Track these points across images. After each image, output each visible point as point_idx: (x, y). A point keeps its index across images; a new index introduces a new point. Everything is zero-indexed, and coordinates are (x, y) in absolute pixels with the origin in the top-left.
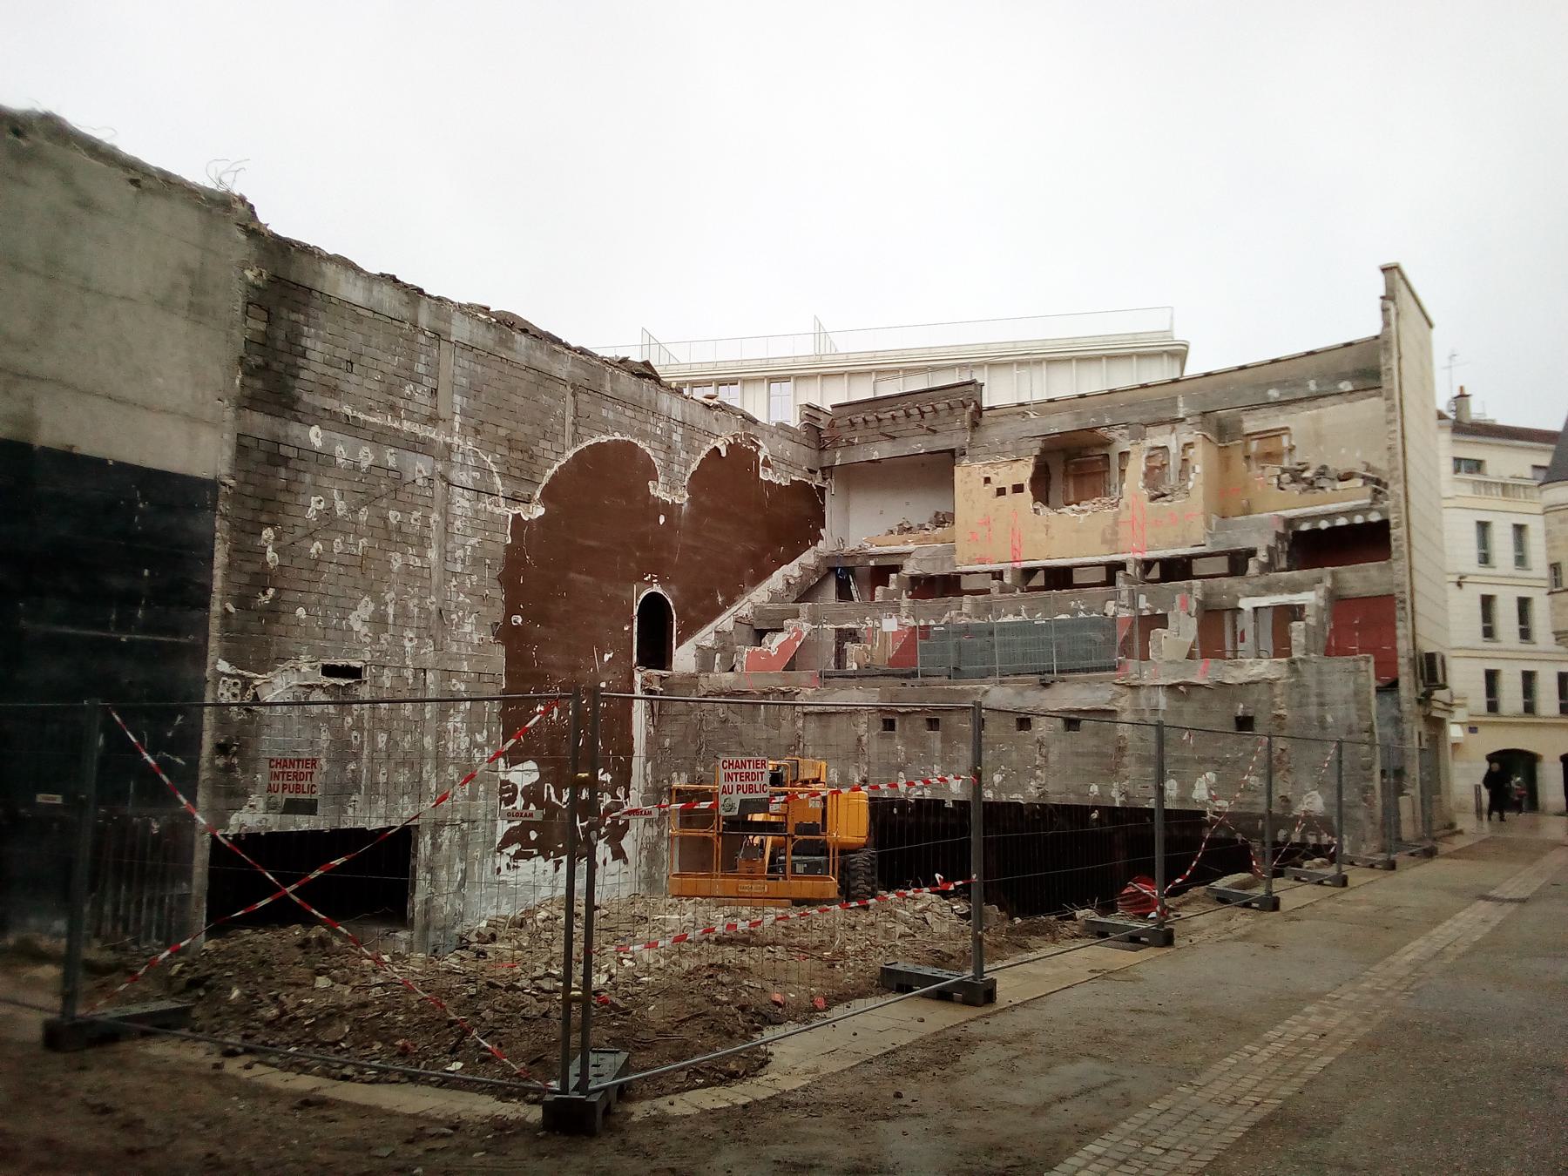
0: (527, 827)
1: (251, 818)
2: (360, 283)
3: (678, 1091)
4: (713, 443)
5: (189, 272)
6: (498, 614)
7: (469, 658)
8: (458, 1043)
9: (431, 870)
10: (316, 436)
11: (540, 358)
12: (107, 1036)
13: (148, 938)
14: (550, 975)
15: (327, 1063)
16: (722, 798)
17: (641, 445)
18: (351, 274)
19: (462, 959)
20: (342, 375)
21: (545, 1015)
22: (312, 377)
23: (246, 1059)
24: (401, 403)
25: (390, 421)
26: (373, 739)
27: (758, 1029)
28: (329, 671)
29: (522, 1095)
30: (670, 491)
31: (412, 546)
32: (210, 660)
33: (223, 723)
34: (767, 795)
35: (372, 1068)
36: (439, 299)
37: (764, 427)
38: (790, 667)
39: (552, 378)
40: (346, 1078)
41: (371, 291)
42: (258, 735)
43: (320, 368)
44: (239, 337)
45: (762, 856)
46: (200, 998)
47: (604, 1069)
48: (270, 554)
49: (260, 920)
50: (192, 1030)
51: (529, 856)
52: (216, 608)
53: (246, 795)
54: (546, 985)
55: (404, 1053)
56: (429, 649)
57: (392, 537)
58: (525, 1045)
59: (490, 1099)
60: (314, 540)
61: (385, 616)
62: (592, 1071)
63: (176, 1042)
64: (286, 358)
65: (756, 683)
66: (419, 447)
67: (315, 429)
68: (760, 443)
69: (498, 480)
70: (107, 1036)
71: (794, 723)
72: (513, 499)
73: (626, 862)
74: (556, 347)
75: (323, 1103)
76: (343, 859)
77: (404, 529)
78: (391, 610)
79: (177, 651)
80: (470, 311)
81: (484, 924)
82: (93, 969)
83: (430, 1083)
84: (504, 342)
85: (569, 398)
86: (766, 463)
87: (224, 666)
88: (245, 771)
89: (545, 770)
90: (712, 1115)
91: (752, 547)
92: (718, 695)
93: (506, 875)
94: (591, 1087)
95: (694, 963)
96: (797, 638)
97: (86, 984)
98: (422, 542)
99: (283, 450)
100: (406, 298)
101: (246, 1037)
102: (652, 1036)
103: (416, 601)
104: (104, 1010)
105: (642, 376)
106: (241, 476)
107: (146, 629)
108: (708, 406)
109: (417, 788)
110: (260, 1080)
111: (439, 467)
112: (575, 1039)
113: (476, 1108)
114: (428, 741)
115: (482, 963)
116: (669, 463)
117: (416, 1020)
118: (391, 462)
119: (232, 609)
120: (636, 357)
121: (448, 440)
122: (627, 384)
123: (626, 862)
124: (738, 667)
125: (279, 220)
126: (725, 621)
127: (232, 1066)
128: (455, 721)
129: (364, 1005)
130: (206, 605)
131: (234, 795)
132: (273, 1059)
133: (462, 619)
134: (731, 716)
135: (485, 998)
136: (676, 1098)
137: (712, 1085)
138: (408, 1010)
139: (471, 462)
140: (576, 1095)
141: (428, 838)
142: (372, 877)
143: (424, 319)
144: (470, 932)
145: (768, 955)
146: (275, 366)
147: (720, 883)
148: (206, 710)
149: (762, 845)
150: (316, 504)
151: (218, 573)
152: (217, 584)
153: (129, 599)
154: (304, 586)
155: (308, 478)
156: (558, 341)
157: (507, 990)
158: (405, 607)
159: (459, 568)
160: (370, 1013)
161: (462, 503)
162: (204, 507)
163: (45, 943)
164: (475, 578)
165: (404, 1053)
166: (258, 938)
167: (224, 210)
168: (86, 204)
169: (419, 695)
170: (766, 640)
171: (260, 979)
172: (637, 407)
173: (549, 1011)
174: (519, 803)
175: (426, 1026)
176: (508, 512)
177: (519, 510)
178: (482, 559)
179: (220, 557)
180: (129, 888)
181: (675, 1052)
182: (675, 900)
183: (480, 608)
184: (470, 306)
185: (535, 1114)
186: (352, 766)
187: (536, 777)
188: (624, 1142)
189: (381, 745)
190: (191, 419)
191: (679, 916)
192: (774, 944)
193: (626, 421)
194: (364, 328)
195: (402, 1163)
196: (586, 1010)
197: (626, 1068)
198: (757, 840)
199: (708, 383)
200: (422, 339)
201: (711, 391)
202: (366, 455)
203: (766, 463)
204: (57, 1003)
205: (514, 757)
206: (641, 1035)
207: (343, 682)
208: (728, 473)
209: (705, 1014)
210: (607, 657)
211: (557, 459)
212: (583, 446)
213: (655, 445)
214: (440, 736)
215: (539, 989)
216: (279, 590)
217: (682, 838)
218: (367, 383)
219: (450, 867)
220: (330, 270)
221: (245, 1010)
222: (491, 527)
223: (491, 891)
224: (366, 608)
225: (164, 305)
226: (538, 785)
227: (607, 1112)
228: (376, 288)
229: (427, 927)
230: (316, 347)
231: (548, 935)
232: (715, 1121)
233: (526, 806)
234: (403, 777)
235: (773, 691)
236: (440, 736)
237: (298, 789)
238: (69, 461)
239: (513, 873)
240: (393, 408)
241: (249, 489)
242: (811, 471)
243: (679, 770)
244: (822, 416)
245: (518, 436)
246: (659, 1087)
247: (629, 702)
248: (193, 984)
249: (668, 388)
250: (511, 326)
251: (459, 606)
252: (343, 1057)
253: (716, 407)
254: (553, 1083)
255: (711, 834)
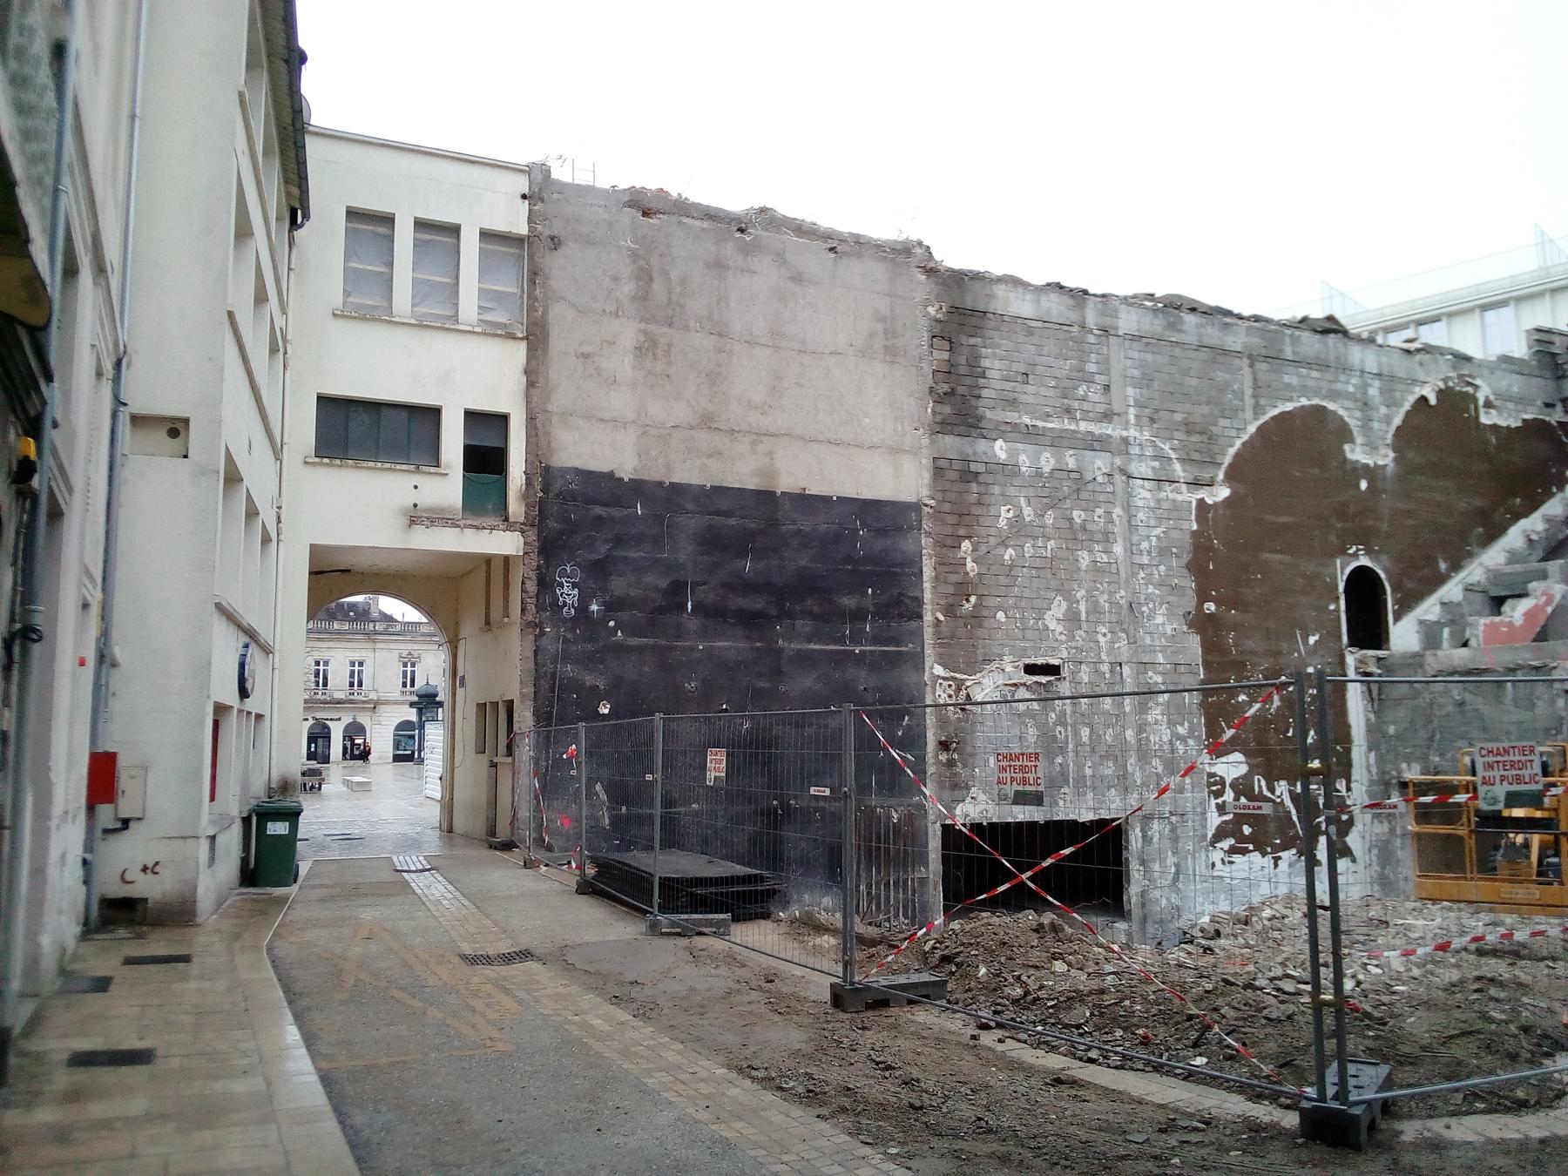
0: (1240, 819)
1: (976, 808)
2: (1029, 297)
3: (1453, 1114)
4: (1419, 391)
5: (882, 319)
6: (1190, 602)
7: (1163, 650)
8: (1199, 1038)
9: (1143, 862)
10: (1000, 449)
11: (1212, 334)
12: (881, 1002)
13: (896, 916)
14: (1288, 976)
15: (1073, 1044)
16: (1482, 790)
17: (1331, 406)
18: (1020, 290)
19: (1189, 953)
20: (1019, 387)
21: (1289, 1017)
22: (993, 394)
23: (999, 1033)
24: (1076, 405)
25: (1069, 425)
26: (1076, 733)
27: (1548, 1055)
28: (1031, 669)
29: (1274, 1098)
30: (1370, 451)
31: (1098, 542)
32: (927, 665)
33: (943, 722)
34: (1540, 787)
35: (1116, 1053)
36: (1104, 296)
37: (1481, 364)
38: (1542, 636)
39: (1226, 352)
40: (1091, 1061)
41: (1038, 302)
42: (974, 732)
43: (998, 385)
44: (928, 370)
45: (1528, 857)
46: (953, 973)
47: (1363, 1080)
48: (970, 565)
49: (993, 904)
50: (949, 1002)
51: (1244, 852)
52: (928, 618)
53: (968, 788)
54: (1288, 986)
55: (1145, 1041)
56: (1122, 643)
57: (1077, 536)
58: (1271, 1047)
59: (1240, 1098)
60: (1007, 547)
61: (1078, 613)
62: (1352, 1082)
63: (936, 1011)
64: (968, 381)
65: (1499, 658)
66: (1097, 445)
67: (1000, 442)
68: (1478, 382)
69: (1178, 467)
70: (881, 1002)
71: (1553, 702)
72: (1196, 484)
73: (1354, 861)
74: (1228, 320)
75: (1074, 1083)
76: (1071, 849)
77: (1089, 527)
78: (1083, 607)
79: (895, 660)
80: (1134, 301)
81: (1206, 919)
82: (863, 941)
83: (1176, 1075)
84: (1173, 326)
85: (1246, 370)
86: (1488, 404)
87: (939, 670)
88: (965, 766)
89: (1255, 761)
90: (1503, 1147)
91: (1479, 502)
92: (1451, 674)
93: (1221, 870)
94: (1352, 1098)
95: (1455, 975)
96: (1548, 603)
97: (859, 955)
98: (1107, 538)
99: (973, 467)
100: (1072, 302)
101: (996, 1012)
102: (1417, 1051)
103: (1106, 597)
104: (875, 978)
105: (1325, 332)
106: (939, 496)
107: (875, 640)
108: (1408, 351)
109: (1123, 782)
110: (1013, 1054)
111: (1118, 461)
112: (1330, 1045)
113: (1226, 1105)
114: (1130, 734)
115: (1210, 959)
116: (1366, 423)
117: (1154, 1011)
118: (1071, 463)
119: (941, 618)
120: (1317, 313)
121: (1125, 434)
122: (1310, 344)
123: (1354, 861)
124: (1473, 642)
125: (951, 257)
126: (1452, 590)
127: (988, 1038)
128: (1155, 714)
129: (1102, 992)
130: (920, 617)
131: (957, 788)
132: (1024, 1036)
133: (1153, 611)
134: (1468, 697)
135: (1223, 994)
136: (1453, 1121)
137: (1496, 1111)
138: (1144, 998)
139: (1149, 452)
140: (1335, 1105)
141: (1138, 830)
142: (1085, 867)
143: (1091, 319)
144: (1193, 926)
145: (1546, 971)
146: (961, 390)
147: (1476, 887)
148: (928, 710)
149: (1526, 845)
150: (1006, 513)
151: (927, 586)
152: (928, 596)
153: (858, 616)
154: (1002, 591)
155: (996, 490)
156: (1229, 313)
157: (1245, 987)
158: (1096, 604)
159: (1145, 560)
160: (1109, 1000)
161: (1143, 494)
162: (911, 528)
163: (823, 917)
164: (1162, 568)
165: (1145, 1041)
166: (995, 920)
167: (906, 256)
168: (797, 278)
169: (1118, 689)
170: (1506, 608)
171: (1003, 960)
172: (1323, 366)
173: (1294, 1014)
174: (1229, 796)
175: (1165, 1017)
176: (1192, 497)
177: (1202, 494)
178: (1168, 549)
179: (928, 573)
180: (878, 872)
181: (1446, 1071)
182: (1419, 904)
183: (1171, 598)
184: (1135, 297)
185: (1291, 1120)
186: (1059, 760)
187: (1244, 769)
188: (1395, 1162)
189: (1085, 739)
190: (895, 450)
191: (1429, 923)
192: (1554, 959)
193: (1311, 383)
194: (1036, 339)
195: (1158, 1151)
196: (1339, 1014)
197: (1388, 1083)
198: (1520, 839)
199: (1404, 326)
200: (1091, 339)
201: (1409, 333)
202: (1047, 461)
203: (1488, 404)
204: (840, 969)
205: (1218, 750)
206: (1406, 1049)
207: (1044, 679)
208: (1441, 425)
209: (1478, 1032)
210: (1312, 640)
211: (1238, 436)
212: (1266, 418)
213: (1348, 404)
214: (1141, 728)
215: (1278, 990)
216: (980, 596)
217: (1419, 837)
218: (1043, 391)
219: (1163, 861)
220: (1000, 290)
221: (993, 988)
222: (1175, 515)
223: (1210, 888)
224: (1059, 608)
225: (864, 353)
226: (1247, 778)
227: (1372, 1126)
228: (1044, 298)
229: (1144, 920)
230: (993, 365)
231: (1276, 934)
232: (1507, 1153)
233: (1237, 799)
234: (1109, 769)
235: (1519, 668)
236: (1141, 728)
237: (1024, 781)
238: (805, 502)
239: (1227, 868)
240: (1068, 411)
241: (947, 507)
242: (1548, 405)
243: (1409, 759)
244: (1557, 339)
245: (1196, 418)
246: (1430, 1107)
247: (1340, 689)
248: (946, 959)
249: (1358, 339)
250: (1178, 308)
251: (1149, 598)
252: (1088, 1040)
253: (1418, 350)
254: (1308, 1089)
255: (1462, 831)
